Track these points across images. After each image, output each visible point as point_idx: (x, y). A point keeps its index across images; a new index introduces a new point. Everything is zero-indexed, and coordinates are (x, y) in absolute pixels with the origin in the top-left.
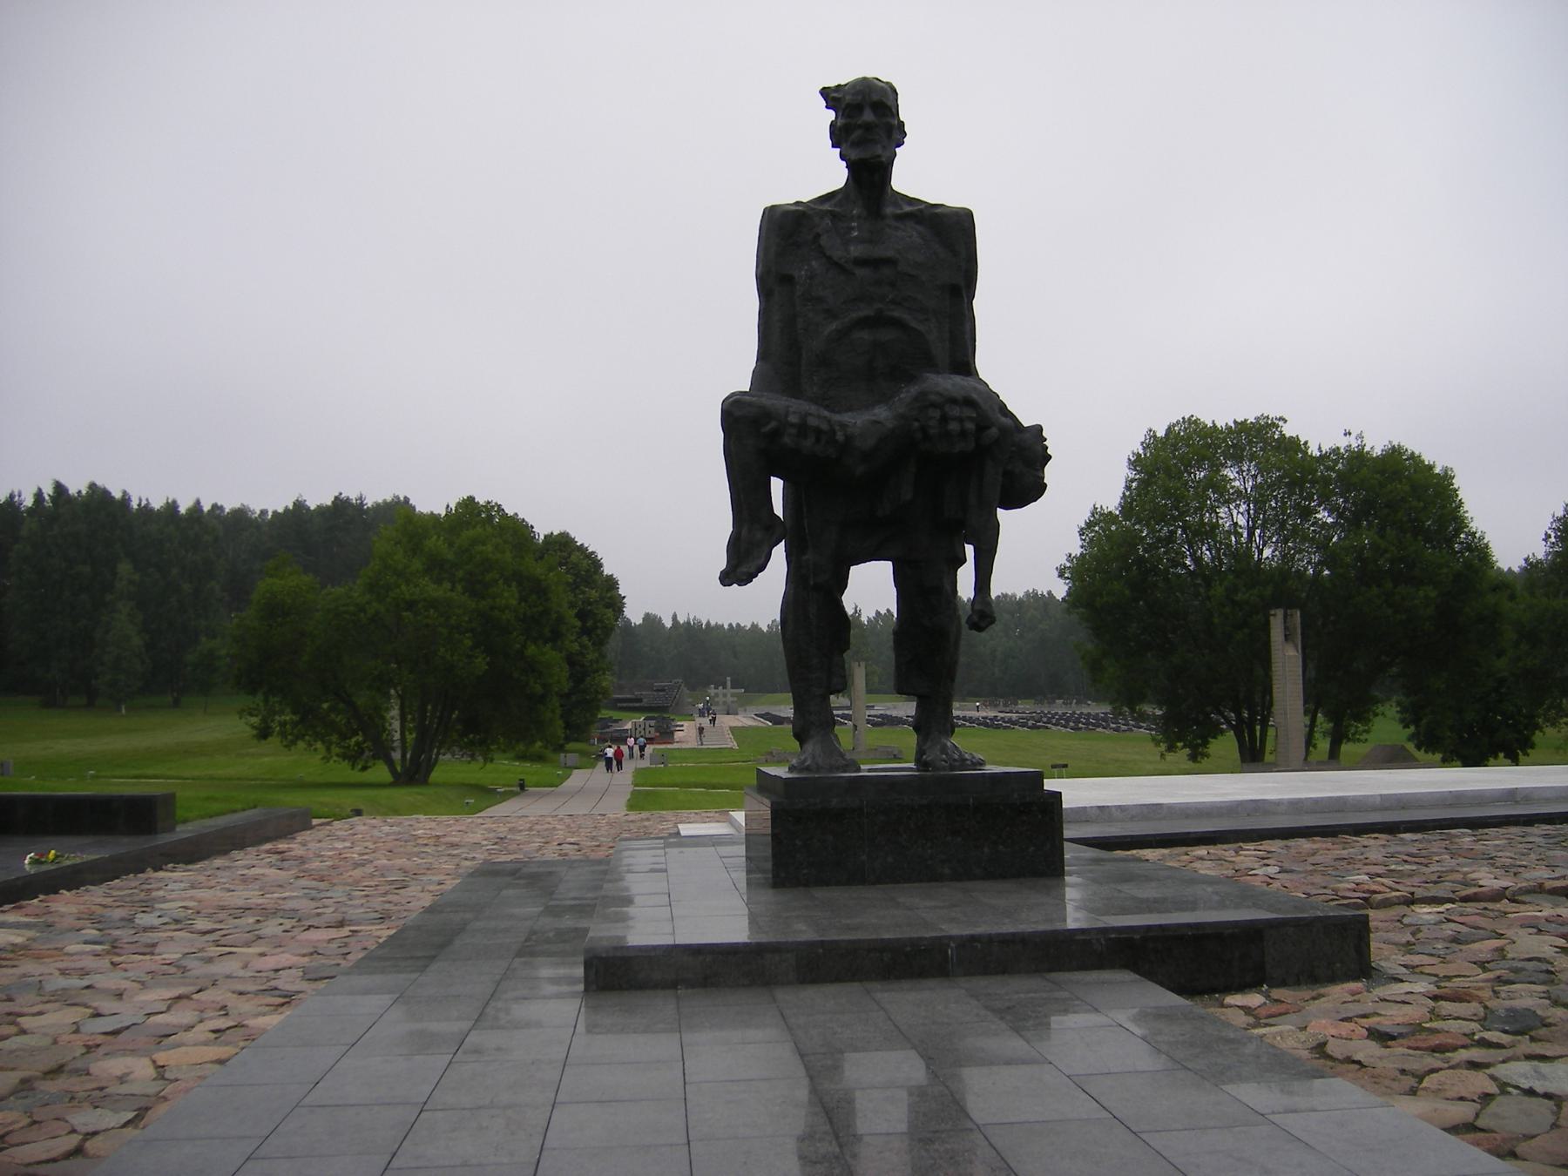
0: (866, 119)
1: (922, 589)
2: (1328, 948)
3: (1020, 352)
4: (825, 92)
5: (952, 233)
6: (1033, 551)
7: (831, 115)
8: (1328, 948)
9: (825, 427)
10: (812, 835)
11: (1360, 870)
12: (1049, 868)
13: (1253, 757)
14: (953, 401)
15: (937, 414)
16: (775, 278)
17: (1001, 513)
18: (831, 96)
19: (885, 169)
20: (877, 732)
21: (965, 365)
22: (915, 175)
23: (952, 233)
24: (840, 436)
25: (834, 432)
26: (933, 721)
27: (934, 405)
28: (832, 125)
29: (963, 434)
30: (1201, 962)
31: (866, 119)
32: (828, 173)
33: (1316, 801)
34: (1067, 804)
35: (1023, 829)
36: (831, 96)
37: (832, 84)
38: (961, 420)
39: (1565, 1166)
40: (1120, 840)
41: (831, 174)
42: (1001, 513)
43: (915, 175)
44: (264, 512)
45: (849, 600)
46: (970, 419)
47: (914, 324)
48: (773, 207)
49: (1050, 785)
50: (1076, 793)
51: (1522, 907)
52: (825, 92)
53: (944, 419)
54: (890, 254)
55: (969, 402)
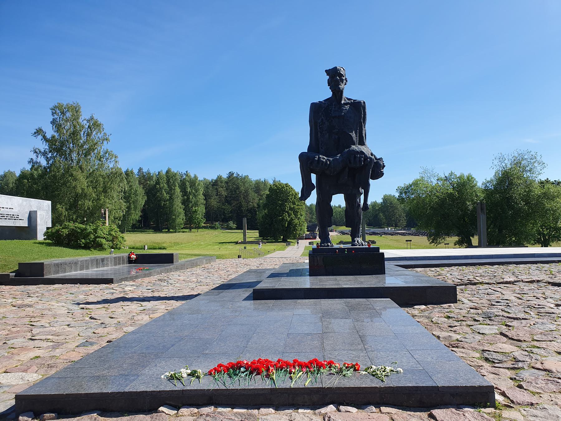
0: (335, 77)
1: (351, 200)
2: (445, 295)
4: (326, 71)
5: (358, 108)
6: (378, 192)
7: (328, 77)
8: (445, 295)
10: (324, 261)
11: (450, 276)
12: (381, 271)
13: (465, 242)
17: (371, 181)
20: (338, 237)
22: (350, 92)
26: (354, 234)
30: (406, 297)
31: (335, 77)
32: (328, 94)
33: (490, 255)
34: (386, 256)
35: (374, 262)
39: (559, 353)
40: (409, 264)
41: (328, 94)
42: (371, 181)
43: (350, 92)
45: (333, 204)
49: (381, 251)
50: (388, 253)
51: (514, 286)
52: (326, 71)
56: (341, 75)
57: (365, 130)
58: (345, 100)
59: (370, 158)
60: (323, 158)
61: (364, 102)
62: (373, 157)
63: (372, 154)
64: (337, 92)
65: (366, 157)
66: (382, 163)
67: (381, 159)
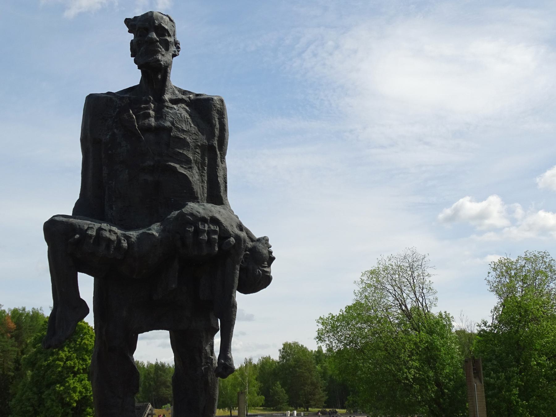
0: (150, 38)
3: (258, 190)
4: (128, 22)
7: (132, 36)
9: (113, 237)
14: (204, 220)
15: (192, 229)
16: (90, 141)
18: (132, 24)
19: (164, 70)
21: (216, 194)
23: (207, 113)
24: (125, 244)
25: (119, 240)
27: (190, 223)
28: (132, 42)
29: (210, 242)
31: (150, 38)
32: (127, 75)
36: (132, 24)
37: (132, 17)
38: (210, 232)
43: (184, 77)
44: (312, 351)
46: (215, 232)
47: (182, 171)
48: (91, 95)
52: (128, 22)
53: (198, 232)
54: (168, 124)
55: (215, 221)
56: (162, 31)
57: (225, 169)
58: (173, 93)
59: (237, 238)
60: (110, 231)
61: (222, 101)
62: (243, 234)
63: (241, 227)
64: (154, 73)
65: (224, 234)
66: (265, 252)
67: (264, 241)
